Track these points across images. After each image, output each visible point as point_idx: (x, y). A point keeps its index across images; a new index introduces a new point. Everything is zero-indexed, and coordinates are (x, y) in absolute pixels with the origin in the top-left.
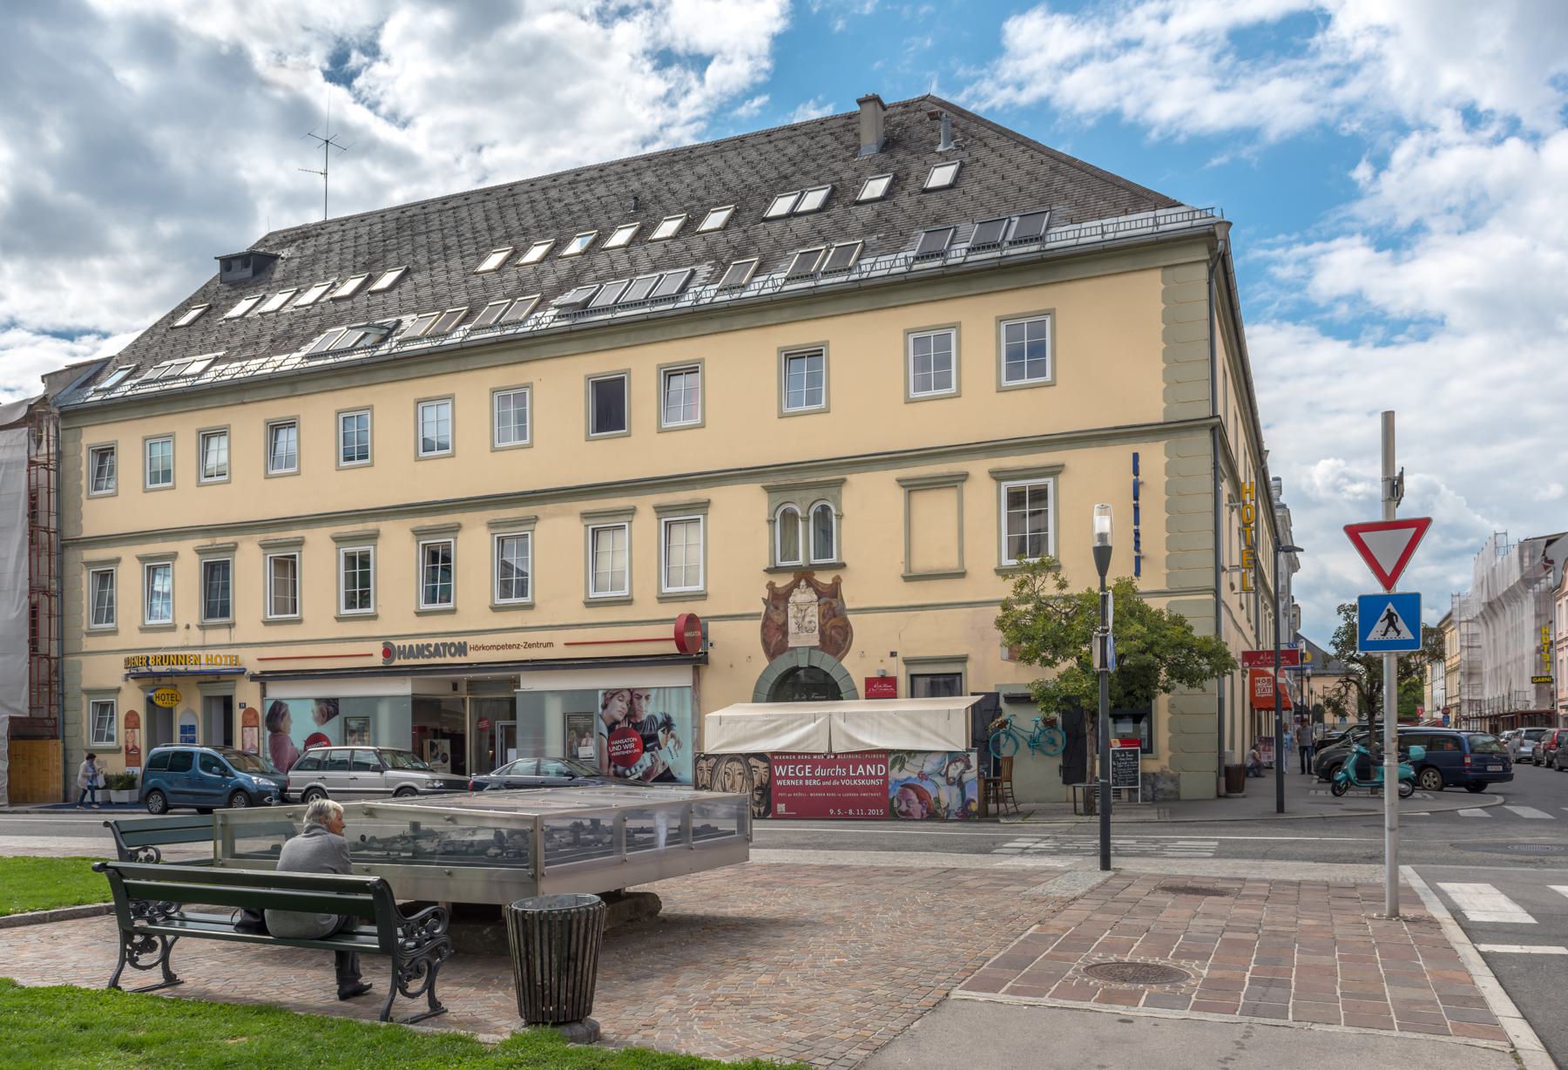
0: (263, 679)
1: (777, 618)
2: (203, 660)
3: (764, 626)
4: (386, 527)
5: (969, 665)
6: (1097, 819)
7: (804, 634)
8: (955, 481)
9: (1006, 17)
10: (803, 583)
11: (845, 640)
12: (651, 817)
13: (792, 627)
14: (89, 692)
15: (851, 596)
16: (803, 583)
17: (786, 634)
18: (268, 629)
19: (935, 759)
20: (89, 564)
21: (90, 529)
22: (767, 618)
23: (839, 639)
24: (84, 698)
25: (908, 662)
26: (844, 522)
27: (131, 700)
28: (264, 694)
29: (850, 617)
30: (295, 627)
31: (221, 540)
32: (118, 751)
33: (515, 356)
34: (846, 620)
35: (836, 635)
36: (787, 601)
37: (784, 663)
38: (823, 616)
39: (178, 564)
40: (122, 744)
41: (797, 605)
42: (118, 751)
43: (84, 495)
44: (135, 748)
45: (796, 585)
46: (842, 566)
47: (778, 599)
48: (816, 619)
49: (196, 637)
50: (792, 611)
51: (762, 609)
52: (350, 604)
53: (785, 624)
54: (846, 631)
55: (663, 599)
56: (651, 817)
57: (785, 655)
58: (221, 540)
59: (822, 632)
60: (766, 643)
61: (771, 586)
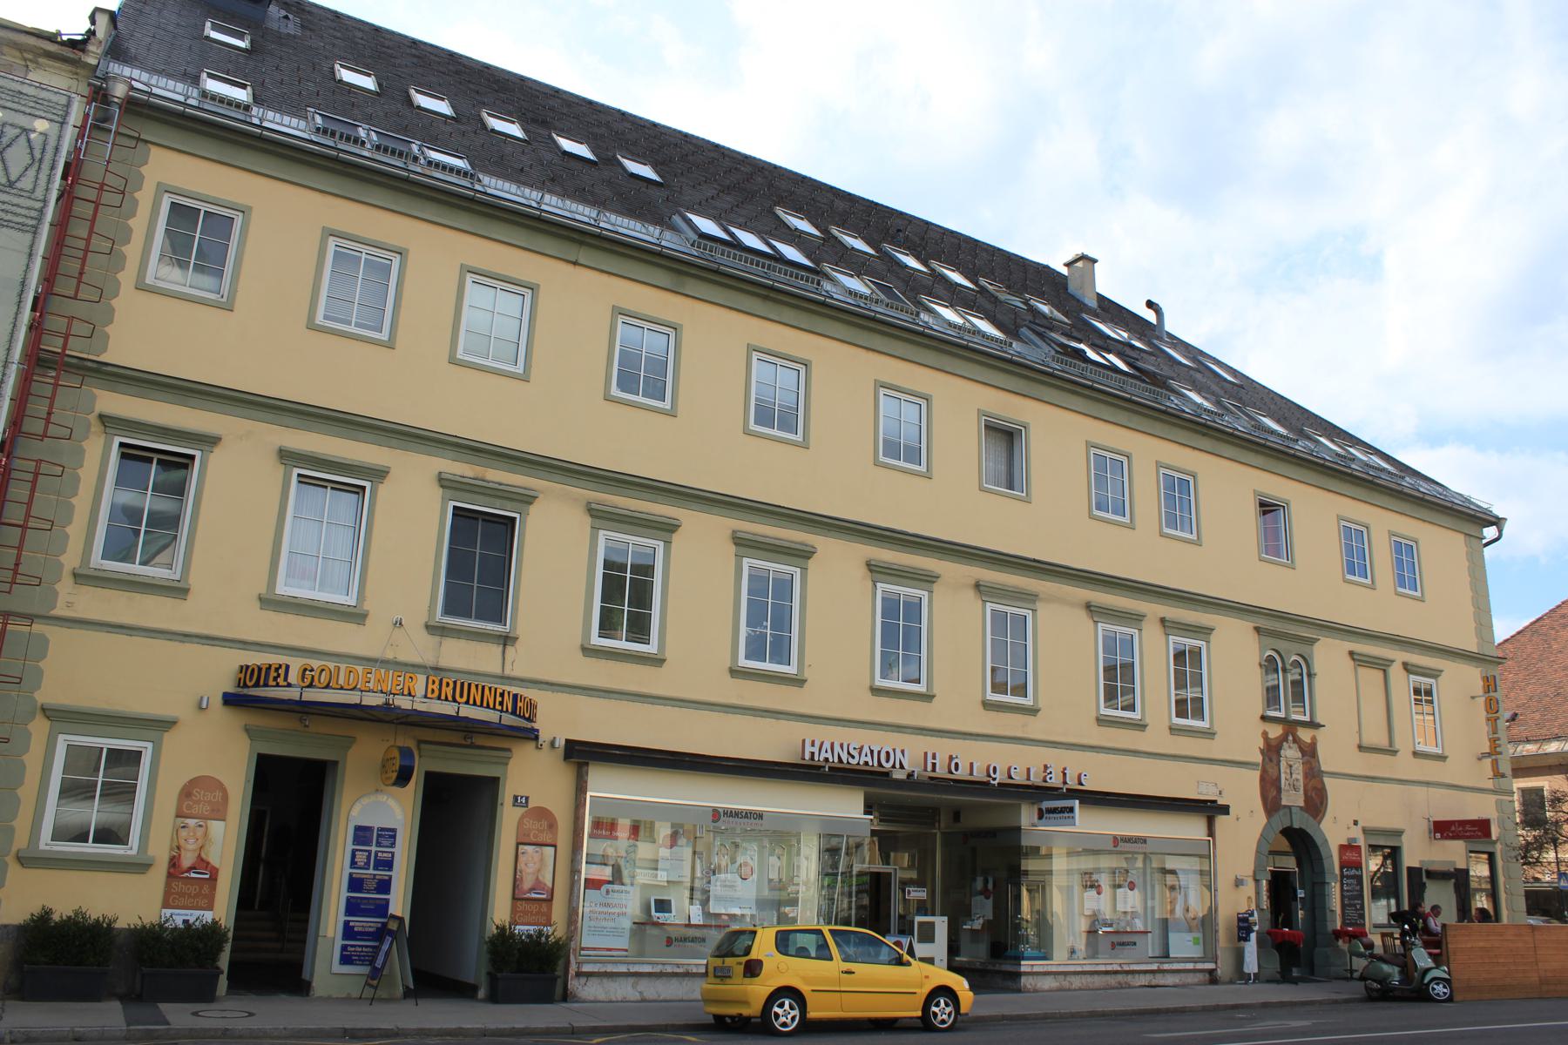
0: (582, 755)
1: (1272, 771)
2: (293, 677)
4: (692, 520)
5: (1404, 838)
8: (355, 482)
14: (61, 717)
17: (1279, 790)
18: (271, 615)
20: (108, 422)
21: (121, 350)
24: (39, 728)
25: (1365, 831)
26: (1317, 681)
27: (225, 757)
28: (580, 788)
29: (1326, 780)
30: (349, 627)
31: (497, 475)
32: (139, 867)
33: (1020, 384)
39: (384, 490)
40: (160, 852)
42: (139, 867)
43: (127, 278)
44: (201, 863)
46: (1317, 726)
47: (1272, 750)
49: (417, 647)
50: (1283, 764)
52: (755, 651)
55: (271, 602)
58: (497, 475)
61: (1265, 734)
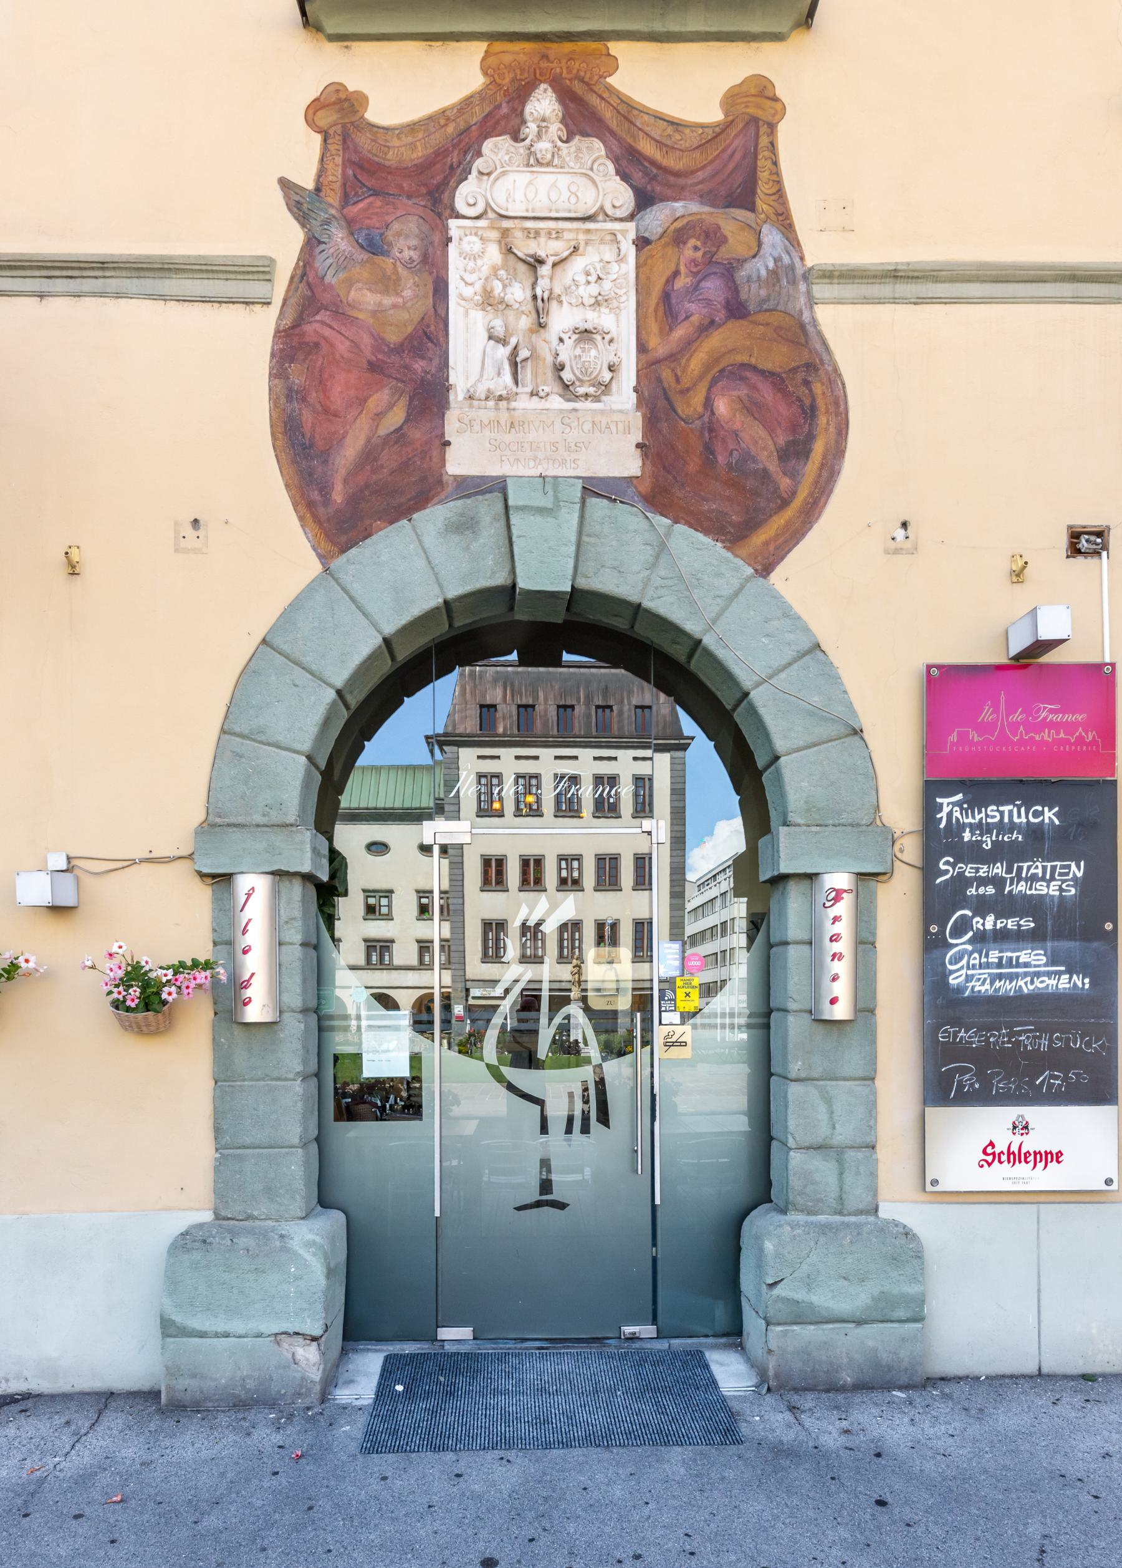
3: (292, 347)
6: (537, 1197)
7: (544, 426)
9: (487, 86)
10: (543, 104)
11: (796, 450)
12: (562, 959)
13: (471, 355)
15: (841, 192)
16: (543, 104)
17: (430, 397)
19: (475, 1123)
22: (310, 296)
23: (761, 444)
29: (840, 324)
34: (801, 336)
35: (746, 425)
36: (438, 204)
37: (417, 570)
38: (660, 306)
41: (499, 220)
45: (496, 114)
48: (621, 323)
50: (470, 258)
51: (284, 241)
53: (430, 335)
54: (803, 404)
56: (562, 959)
57: (433, 519)
59: (657, 403)
60: (301, 446)
61: (337, 114)
